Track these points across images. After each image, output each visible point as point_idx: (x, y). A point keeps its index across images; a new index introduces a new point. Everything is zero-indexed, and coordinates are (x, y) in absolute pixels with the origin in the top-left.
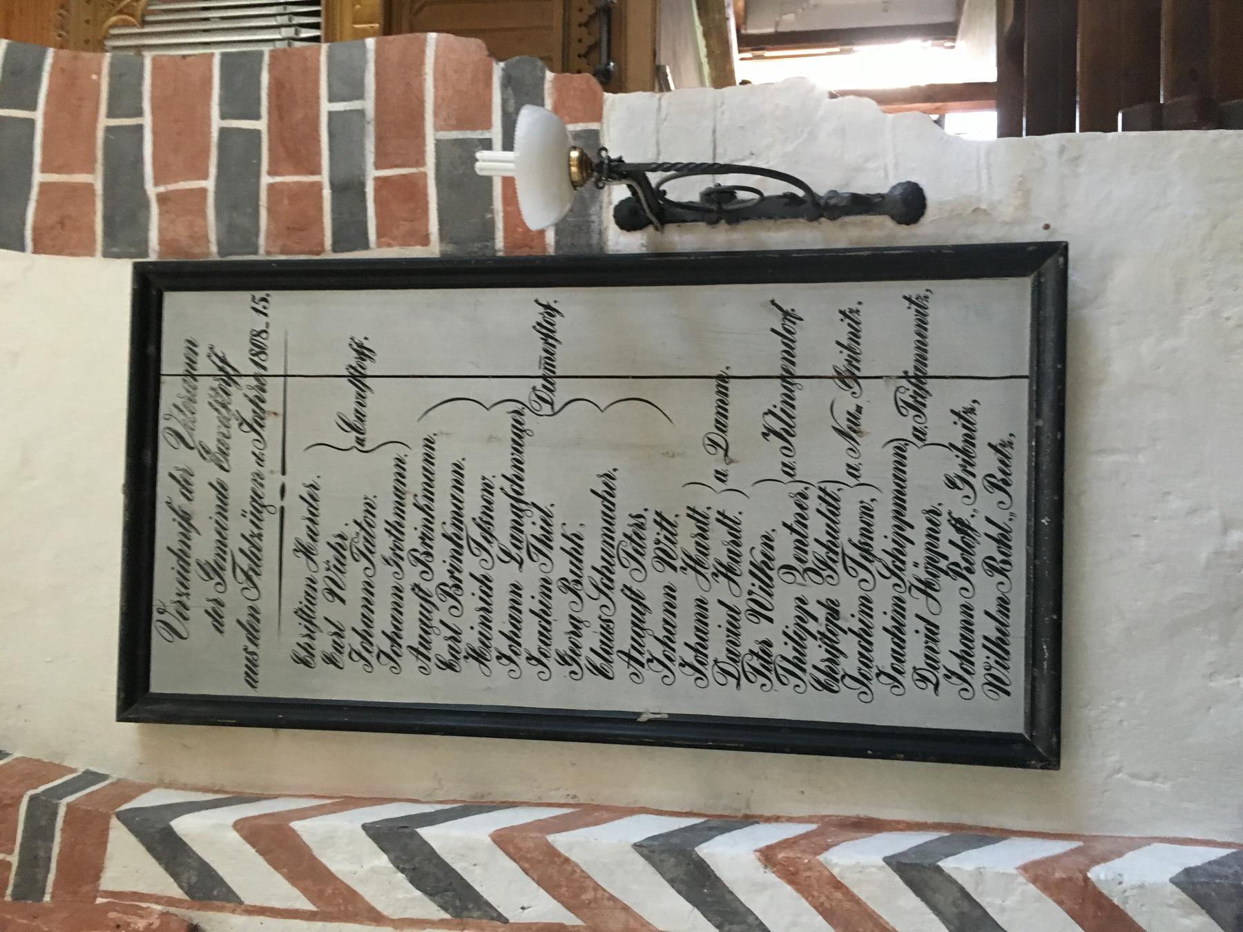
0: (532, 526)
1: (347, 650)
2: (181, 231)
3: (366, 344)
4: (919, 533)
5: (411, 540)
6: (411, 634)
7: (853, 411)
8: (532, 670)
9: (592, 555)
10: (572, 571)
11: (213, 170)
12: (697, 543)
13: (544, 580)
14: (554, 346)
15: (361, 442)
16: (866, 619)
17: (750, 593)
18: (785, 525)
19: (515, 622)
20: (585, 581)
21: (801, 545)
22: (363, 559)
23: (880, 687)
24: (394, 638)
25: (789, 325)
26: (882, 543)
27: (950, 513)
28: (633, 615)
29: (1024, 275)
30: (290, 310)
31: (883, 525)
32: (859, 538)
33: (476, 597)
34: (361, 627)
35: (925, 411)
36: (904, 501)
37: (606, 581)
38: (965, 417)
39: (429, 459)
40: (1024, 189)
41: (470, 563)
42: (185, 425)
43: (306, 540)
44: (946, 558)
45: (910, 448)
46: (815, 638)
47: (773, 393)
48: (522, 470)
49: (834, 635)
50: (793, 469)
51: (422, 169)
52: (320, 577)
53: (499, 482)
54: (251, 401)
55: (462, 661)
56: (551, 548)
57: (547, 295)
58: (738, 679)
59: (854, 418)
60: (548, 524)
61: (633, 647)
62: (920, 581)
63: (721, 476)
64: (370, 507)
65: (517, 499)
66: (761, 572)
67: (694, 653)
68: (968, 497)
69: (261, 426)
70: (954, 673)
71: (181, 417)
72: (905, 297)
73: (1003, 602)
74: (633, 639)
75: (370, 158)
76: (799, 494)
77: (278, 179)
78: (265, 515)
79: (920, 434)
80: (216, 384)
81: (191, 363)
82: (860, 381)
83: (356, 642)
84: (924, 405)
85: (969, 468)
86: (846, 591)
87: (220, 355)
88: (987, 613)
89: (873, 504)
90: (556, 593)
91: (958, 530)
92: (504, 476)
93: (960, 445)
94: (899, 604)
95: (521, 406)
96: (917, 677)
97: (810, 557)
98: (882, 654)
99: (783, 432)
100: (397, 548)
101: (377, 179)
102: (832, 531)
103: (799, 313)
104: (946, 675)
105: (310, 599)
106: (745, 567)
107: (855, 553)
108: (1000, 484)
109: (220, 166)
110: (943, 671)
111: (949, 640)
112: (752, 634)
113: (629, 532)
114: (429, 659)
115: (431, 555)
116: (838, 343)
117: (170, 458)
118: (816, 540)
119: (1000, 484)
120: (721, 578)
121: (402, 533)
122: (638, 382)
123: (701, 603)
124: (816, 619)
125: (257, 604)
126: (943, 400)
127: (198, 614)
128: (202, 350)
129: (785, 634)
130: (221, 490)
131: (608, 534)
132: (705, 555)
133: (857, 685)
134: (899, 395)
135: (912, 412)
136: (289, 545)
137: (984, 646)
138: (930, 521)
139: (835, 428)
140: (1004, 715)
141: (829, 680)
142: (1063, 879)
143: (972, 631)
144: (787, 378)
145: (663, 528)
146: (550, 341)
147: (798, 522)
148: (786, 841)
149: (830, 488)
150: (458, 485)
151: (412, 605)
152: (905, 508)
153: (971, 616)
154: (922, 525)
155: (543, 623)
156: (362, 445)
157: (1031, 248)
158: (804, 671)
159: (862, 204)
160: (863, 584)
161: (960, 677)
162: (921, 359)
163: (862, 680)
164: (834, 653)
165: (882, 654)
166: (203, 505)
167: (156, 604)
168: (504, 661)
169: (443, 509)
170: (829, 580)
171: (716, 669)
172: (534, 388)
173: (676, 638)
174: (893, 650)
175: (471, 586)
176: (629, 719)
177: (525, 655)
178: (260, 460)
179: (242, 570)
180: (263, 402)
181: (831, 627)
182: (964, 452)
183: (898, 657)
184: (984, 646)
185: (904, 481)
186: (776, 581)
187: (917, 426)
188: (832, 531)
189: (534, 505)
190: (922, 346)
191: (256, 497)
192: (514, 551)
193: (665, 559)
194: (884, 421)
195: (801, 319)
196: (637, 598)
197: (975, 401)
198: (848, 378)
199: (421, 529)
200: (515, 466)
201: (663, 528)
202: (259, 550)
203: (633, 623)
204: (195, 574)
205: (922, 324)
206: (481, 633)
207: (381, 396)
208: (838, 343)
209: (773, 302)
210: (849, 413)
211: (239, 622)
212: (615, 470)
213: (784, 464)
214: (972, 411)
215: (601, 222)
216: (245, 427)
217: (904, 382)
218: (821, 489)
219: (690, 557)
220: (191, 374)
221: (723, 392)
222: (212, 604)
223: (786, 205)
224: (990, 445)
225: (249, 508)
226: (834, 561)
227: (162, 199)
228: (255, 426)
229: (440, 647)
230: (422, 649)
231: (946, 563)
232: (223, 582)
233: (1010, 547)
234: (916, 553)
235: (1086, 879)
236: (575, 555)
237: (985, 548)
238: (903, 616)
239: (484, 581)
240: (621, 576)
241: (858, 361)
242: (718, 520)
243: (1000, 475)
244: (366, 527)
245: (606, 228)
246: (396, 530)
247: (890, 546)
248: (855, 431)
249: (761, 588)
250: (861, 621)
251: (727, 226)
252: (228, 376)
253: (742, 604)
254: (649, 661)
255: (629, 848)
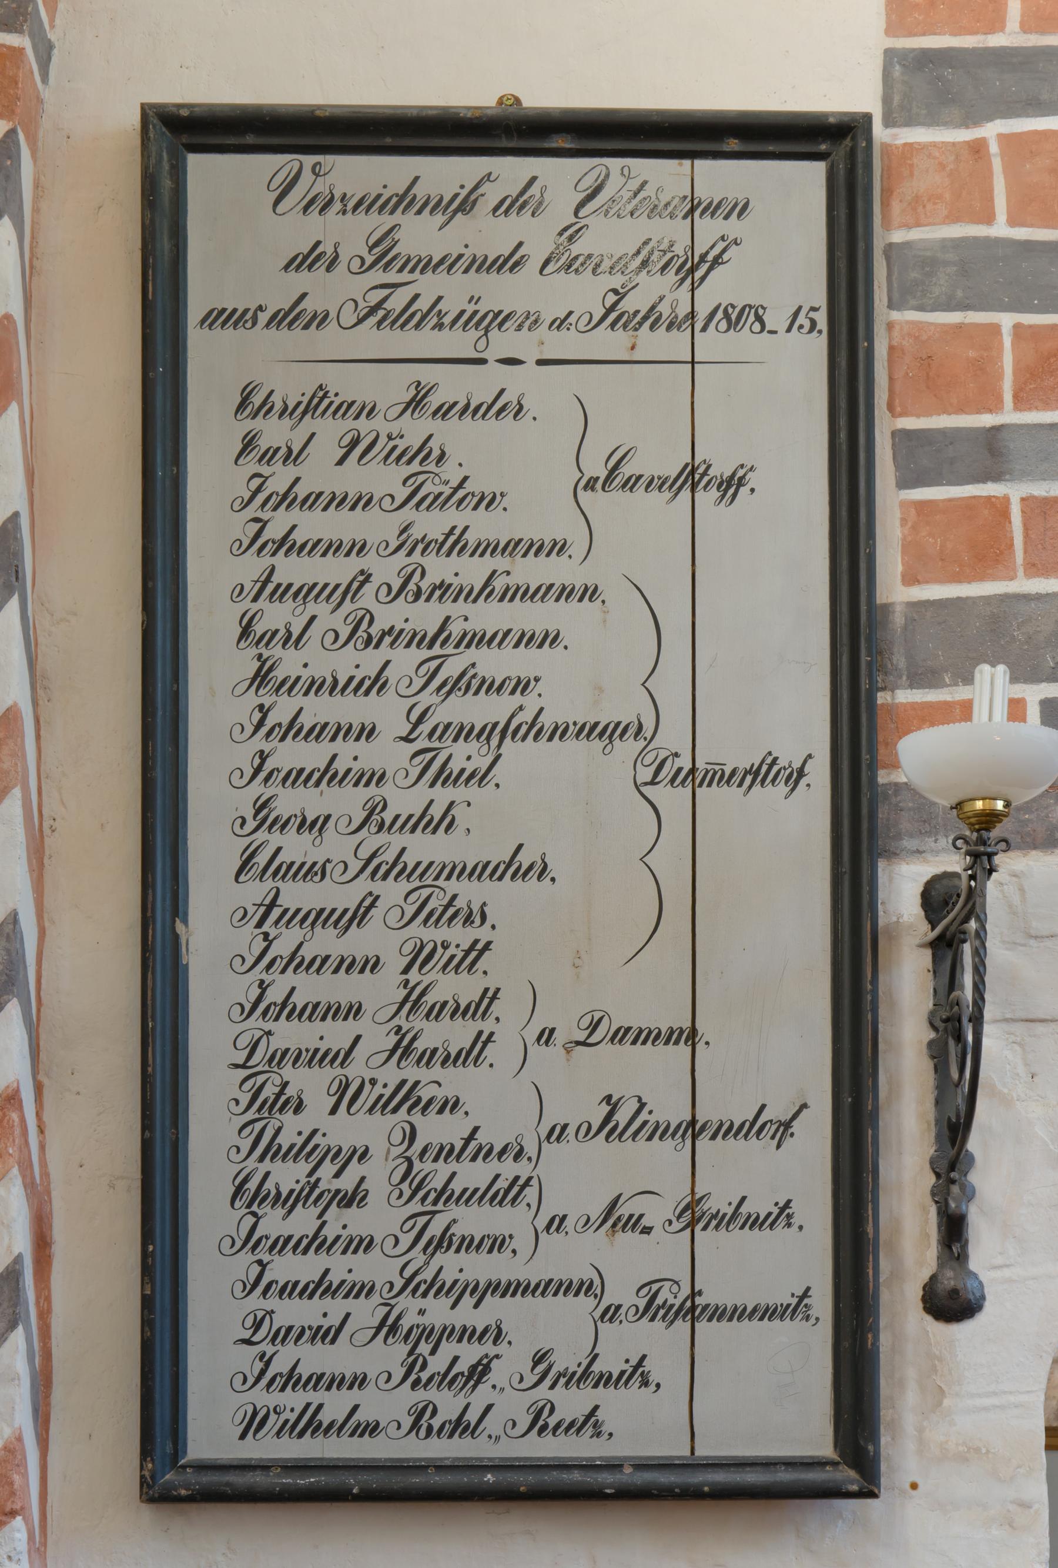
0: (463, 755)
1: (265, 470)
2: (925, 180)
3: (744, 491)
4: (466, 1315)
5: (439, 568)
6: (293, 570)
7: (645, 1222)
8: (244, 756)
9: (421, 848)
10: (397, 817)
11: (1021, 233)
12: (445, 1004)
13: (383, 775)
14: (740, 785)
15: (591, 485)
16: (340, 1246)
17: (373, 1082)
18: (476, 1129)
19: (316, 733)
20: (383, 838)
21: (446, 1153)
22: (408, 491)
23: (244, 1265)
24: (285, 544)
25: (771, 1129)
26: (452, 1265)
27: (497, 1356)
28: (333, 911)
29: (836, 1446)
30: (807, 359)
31: (480, 1267)
32: (459, 1234)
33: (354, 672)
34: (301, 491)
35: (645, 1320)
36: (513, 1295)
37: (384, 868)
38: (637, 1373)
39: (565, 593)
40: (969, 1454)
41: (405, 661)
42: (612, 200)
43: (434, 401)
44: (433, 1352)
45: (591, 1302)
46: (310, 1174)
47: (672, 1109)
48: (550, 739)
49: (316, 1202)
50: (558, 1139)
51: (1021, 572)
52: (378, 423)
53: (531, 703)
54: (653, 308)
55: (254, 651)
56: (432, 785)
57: (820, 773)
58: (243, 1066)
59: (635, 1224)
60: (468, 780)
61: (286, 911)
62: (399, 1317)
63: (546, 1036)
64: (488, 501)
65: (507, 731)
66: (406, 1097)
67: (280, 1001)
68: (521, 1380)
69: (613, 325)
70: (268, 1364)
71: (626, 195)
72: (808, 1289)
73: (372, 1429)
74: (298, 911)
75: (1040, 489)
76: (522, 1150)
77: (1007, 341)
78: (473, 334)
79: (611, 1314)
80: (679, 250)
81: (712, 209)
82: (689, 1230)
83: (278, 484)
84: (652, 1319)
85: (562, 1380)
86: (381, 1216)
87: (725, 257)
88: (355, 1408)
89: (508, 1253)
90: (363, 794)
91: (473, 1368)
92: (541, 709)
93: (596, 1368)
94: (365, 1290)
95: (649, 735)
96: (260, 1315)
97: (428, 1166)
98: (287, 1268)
99: (609, 1126)
100: (426, 545)
101: (1006, 499)
102: (467, 1197)
103: (788, 1143)
104: (264, 1354)
105: (344, 409)
106: (412, 1073)
107: (436, 1228)
108: (541, 1423)
109: (1027, 246)
110: (270, 1350)
111: (314, 1358)
112: (313, 1084)
113: (459, 903)
114: (255, 599)
115: (416, 599)
116: (744, 1199)
117: (561, 176)
118: (454, 1174)
119: (541, 1423)
120: (393, 1039)
121: (448, 555)
122: (685, 913)
123: (355, 1011)
124: (337, 1175)
125: (332, 326)
126: (662, 1344)
127: (315, 228)
128: (733, 227)
129: (315, 1132)
130: (510, 262)
131: (455, 871)
132: (428, 1015)
133: (243, 1235)
134: (667, 1284)
135: (642, 1303)
136: (426, 374)
137: (308, 1405)
138: (486, 1331)
139: (620, 1196)
140: (211, 1432)
141: (248, 1195)
142: (12, 1484)
143: (329, 1388)
144: (693, 1129)
145: (467, 953)
146: (749, 778)
147: (480, 1149)
148: (27, 1130)
149: (531, 1193)
150: (525, 640)
151: (338, 570)
152: (503, 1296)
153: (350, 1387)
154: (479, 1319)
155: (316, 775)
156: (585, 488)
157: (871, 1448)
158: (261, 1159)
159: (953, 1230)
160: (392, 1240)
161: (263, 1372)
162: (719, 1314)
163: (251, 1241)
164: (289, 1202)
165: (287, 1268)
166: (490, 234)
167: (328, 160)
168: (257, 716)
169: (488, 616)
170: (397, 1193)
171: (259, 1033)
172: (676, 755)
173: (302, 975)
174: (297, 1283)
175: (370, 662)
176: (178, 907)
177: (267, 747)
178: (560, 324)
179: (385, 299)
180: (652, 328)
181: (326, 1197)
182: (586, 1373)
183: (288, 1290)
184: (308, 1405)
185: (543, 1294)
186: (391, 1119)
187: (623, 1311)
188: (467, 1197)
189: (498, 758)
190: (738, 1314)
191: (500, 318)
192: (425, 728)
193: (420, 957)
194: (627, 1265)
195: (778, 1146)
196: (360, 915)
197: (658, 1386)
198: (693, 1215)
199: (456, 582)
200: (556, 728)
201: (467, 953)
202: (417, 326)
203: (322, 910)
204: (377, 222)
205: (769, 1313)
206: (298, 678)
207: (663, 514)
208: (744, 1199)
209: (804, 1106)
210: (641, 1216)
211: (304, 296)
212: (553, 880)
213: (565, 1127)
214: (645, 1383)
215: (936, 852)
216: (611, 298)
217: (686, 1291)
218: (530, 1179)
219: (423, 994)
220: (693, 208)
221: (671, 1037)
222: (330, 251)
223: (949, 1118)
224: (596, 1407)
225: (483, 307)
226: (424, 1199)
227: (978, 148)
228: (613, 315)
229: (275, 616)
230: (270, 587)
231: (426, 1353)
232: (366, 268)
233: (451, 1436)
234: (438, 1312)
235: (13, 1514)
236: (422, 822)
237: (448, 1404)
238: (346, 1296)
239: (378, 683)
240: (392, 891)
241: (717, 1227)
242: (480, 1033)
243: (552, 1422)
244: (458, 495)
245: (926, 861)
246: (455, 543)
247: (448, 1277)
248: (614, 1225)
249: (381, 1096)
250: (338, 1238)
251: (926, 1041)
252: (693, 269)
253: (356, 1070)
254: (266, 935)
255: (11, 906)
